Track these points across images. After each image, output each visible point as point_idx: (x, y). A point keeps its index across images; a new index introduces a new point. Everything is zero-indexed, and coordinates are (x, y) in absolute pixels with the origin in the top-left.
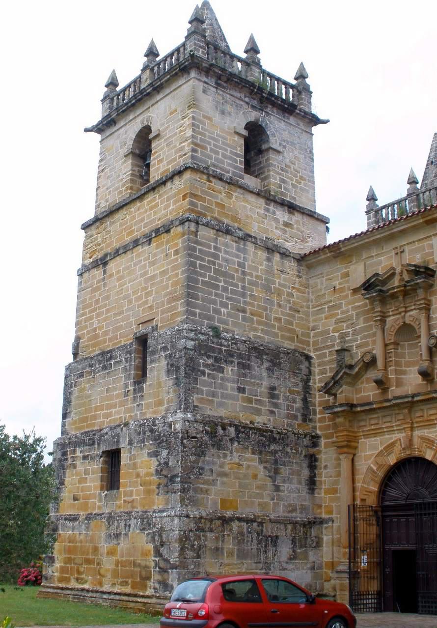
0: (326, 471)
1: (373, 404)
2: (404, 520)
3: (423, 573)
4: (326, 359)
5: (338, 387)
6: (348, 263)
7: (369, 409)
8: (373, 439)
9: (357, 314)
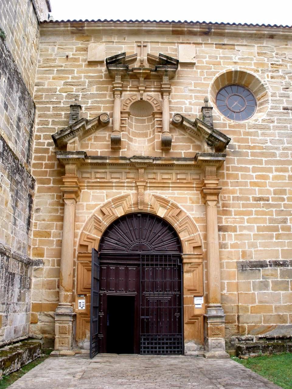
0: (38, 214)
1: (106, 159)
2: (123, 268)
3: (148, 317)
4: (48, 113)
5: (72, 137)
6: (86, 41)
7: (99, 163)
8: (98, 191)
9: (90, 82)
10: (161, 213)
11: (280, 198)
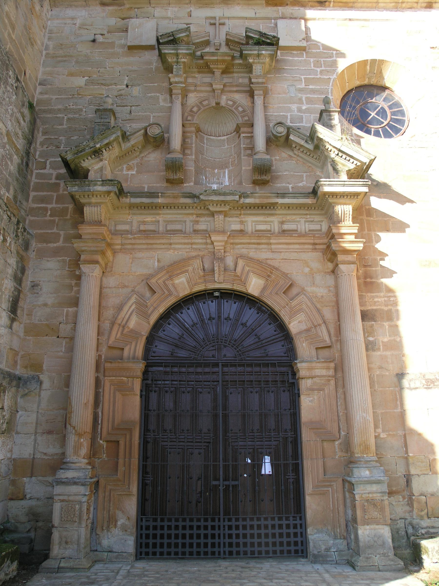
10: (254, 286)
11: (47, 241)
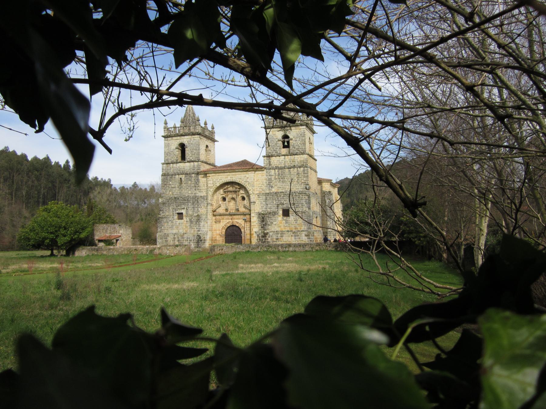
10: (237, 225)
